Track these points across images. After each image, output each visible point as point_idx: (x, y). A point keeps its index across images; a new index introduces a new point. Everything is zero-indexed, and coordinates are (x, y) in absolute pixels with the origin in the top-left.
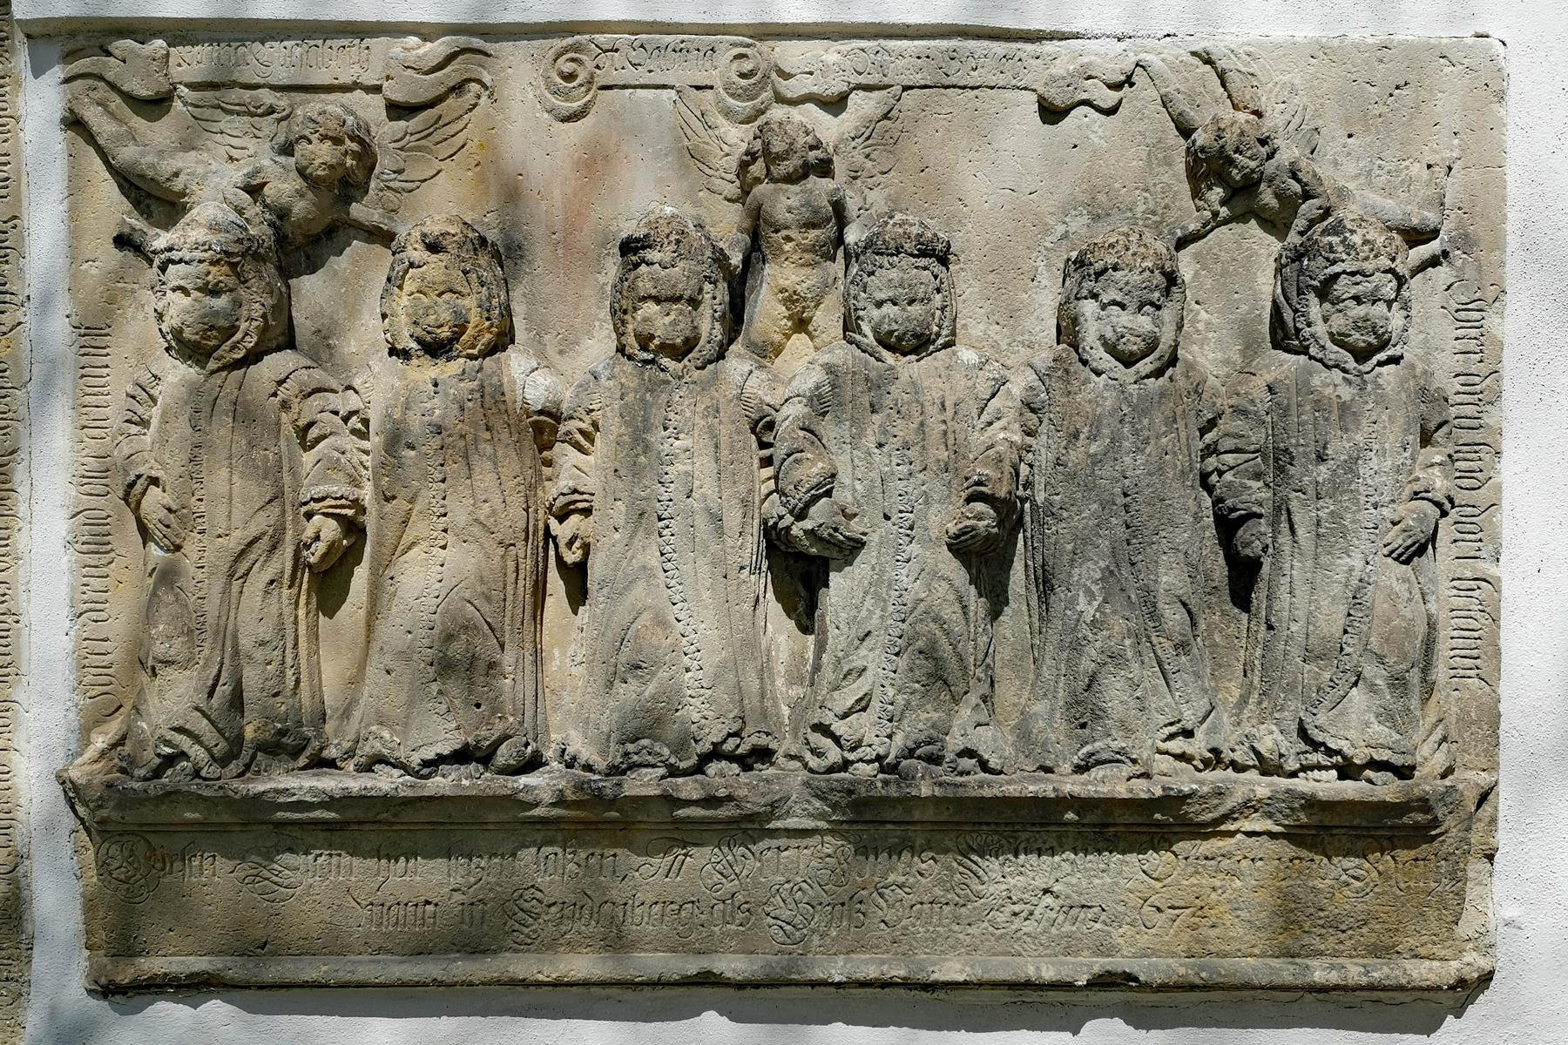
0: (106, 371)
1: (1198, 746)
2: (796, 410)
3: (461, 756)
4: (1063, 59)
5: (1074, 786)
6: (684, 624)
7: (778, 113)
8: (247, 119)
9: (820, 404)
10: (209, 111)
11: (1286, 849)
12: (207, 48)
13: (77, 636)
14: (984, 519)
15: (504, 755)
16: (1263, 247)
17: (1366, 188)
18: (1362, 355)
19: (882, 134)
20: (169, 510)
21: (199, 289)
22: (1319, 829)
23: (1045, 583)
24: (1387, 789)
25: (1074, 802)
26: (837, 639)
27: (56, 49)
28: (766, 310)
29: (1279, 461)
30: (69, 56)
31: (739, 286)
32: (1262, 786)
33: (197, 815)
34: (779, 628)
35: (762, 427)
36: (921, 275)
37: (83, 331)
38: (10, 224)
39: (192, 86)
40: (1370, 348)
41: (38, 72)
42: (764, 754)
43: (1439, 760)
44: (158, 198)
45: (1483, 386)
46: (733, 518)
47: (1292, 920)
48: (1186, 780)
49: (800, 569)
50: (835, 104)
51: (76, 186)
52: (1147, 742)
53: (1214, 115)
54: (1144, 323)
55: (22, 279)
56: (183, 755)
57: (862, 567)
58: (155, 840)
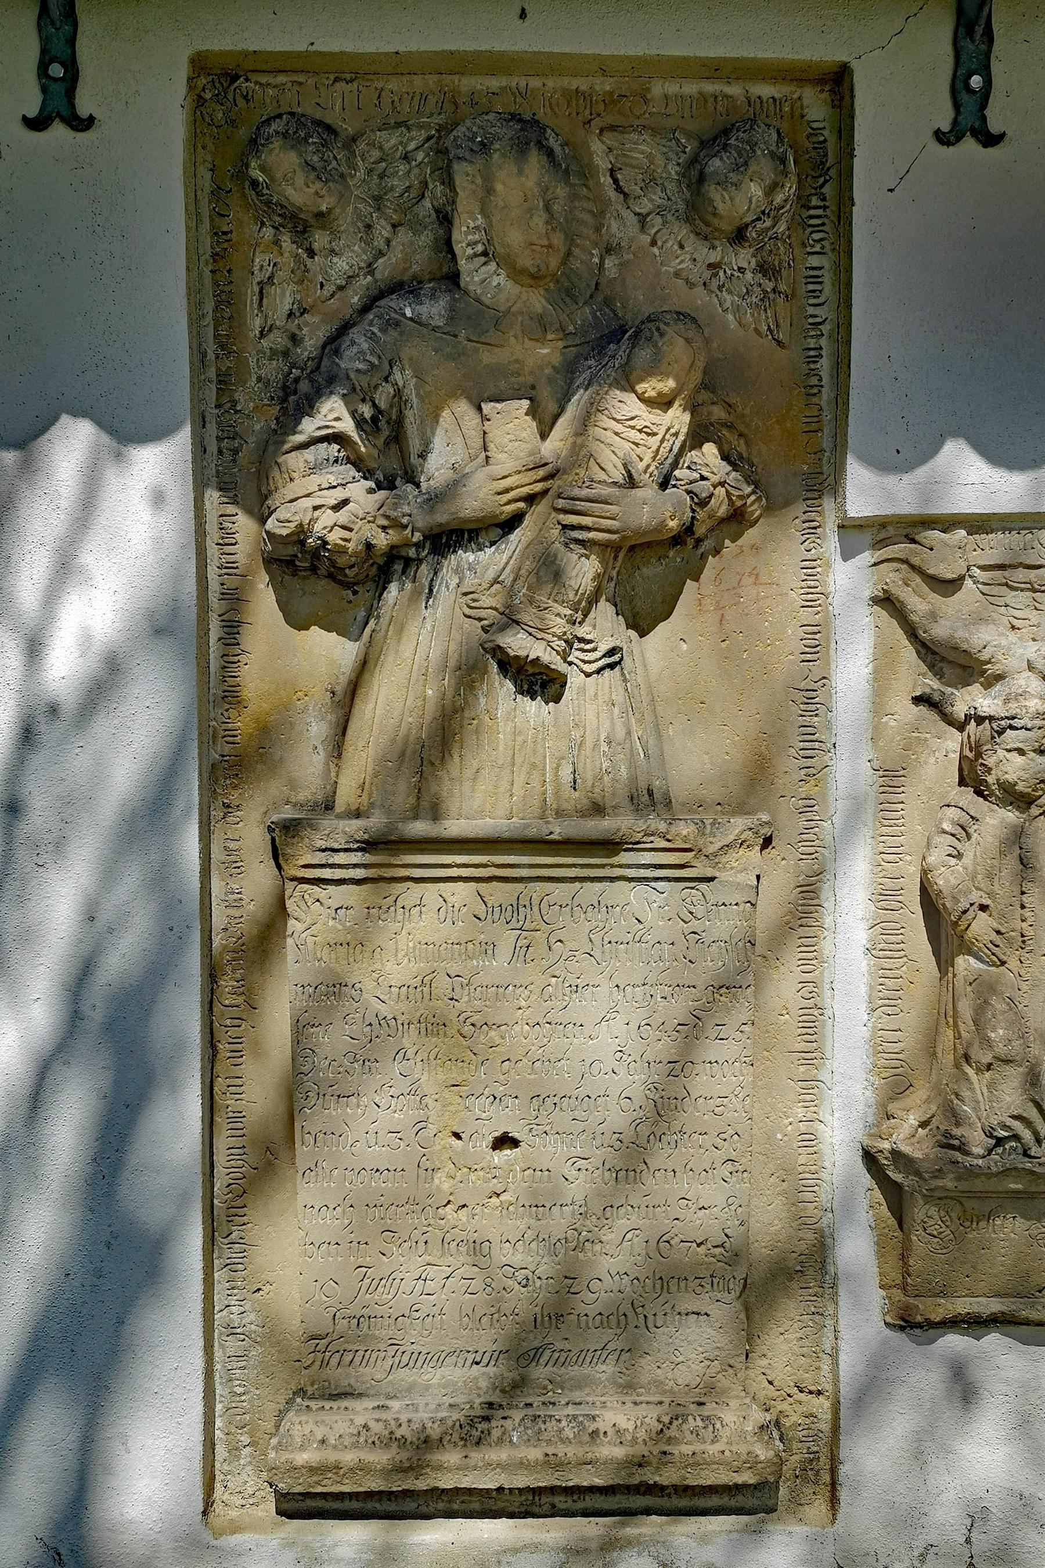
0: (901, 806)
8: (1029, 594)
10: (997, 588)
12: (1000, 535)
13: (874, 1027)
20: (998, 932)
21: (1034, 751)
27: (867, 537)
30: (879, 544)
33: (1020, 1186)
37: (881, 773)
38: (820, 683)
39: (984, 568)
41: (846, 556)
44: (950, 662)
55: (830, 729)
56: (1016, 1137)
58: (969, 1204)
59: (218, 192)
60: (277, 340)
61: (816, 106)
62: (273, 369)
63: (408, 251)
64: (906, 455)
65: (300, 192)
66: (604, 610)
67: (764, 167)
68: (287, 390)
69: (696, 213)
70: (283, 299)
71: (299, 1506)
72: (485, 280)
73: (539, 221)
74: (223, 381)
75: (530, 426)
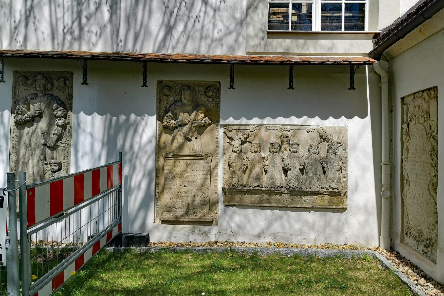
1: (320, 187)
2: (286, 157)
3: (257, 186)
4: (309, 128)
5: (309, 190)
6: (280, 179)
7: (284, 132)
9: (288, 157)
11: (328, 196)
14: (302, 167)
15: (261, 186)
16: (326, 144)
17: (335, 139)
18: (334, 154)
19: (294, 135)
22: (331, 194)
23: (307, 173)
24: (336, 190)
25: (309, 191)
26: (289, 177)
28: (283, 149)
29: (327, 163)
31: (280, 147)
32: (326, 190)
34: (283, 176)
35: (283, 159)
36: (295, 146)
40: (335, 153)
42: (282, 187)
43: (341, 188)
45: (346, 155)
46: (280, 167)
47: (330, 202)
48: (319, 190)
49: (286, 171)
50: (289, 131)
51: (224, 138)
52: (316, 186)
53: (321, 132)
54: (316, 151)
57: (291, 171)
59: (160, 92)
60: (165, 106)
61: (218, 85)
62: (164, 109)
63: (177, 98)
64: (226, 119)
65: (167, 93)
66: (196, 133)
67: (211, 91)
68: (165, 111)
69: (206, 95)
70: (165, 102)
71: (163, 222)
72: (185, 101)
73: (190, 96)
74: (159, 110)
75: (188, 115)
